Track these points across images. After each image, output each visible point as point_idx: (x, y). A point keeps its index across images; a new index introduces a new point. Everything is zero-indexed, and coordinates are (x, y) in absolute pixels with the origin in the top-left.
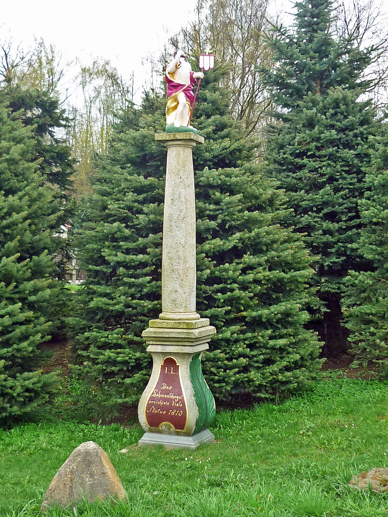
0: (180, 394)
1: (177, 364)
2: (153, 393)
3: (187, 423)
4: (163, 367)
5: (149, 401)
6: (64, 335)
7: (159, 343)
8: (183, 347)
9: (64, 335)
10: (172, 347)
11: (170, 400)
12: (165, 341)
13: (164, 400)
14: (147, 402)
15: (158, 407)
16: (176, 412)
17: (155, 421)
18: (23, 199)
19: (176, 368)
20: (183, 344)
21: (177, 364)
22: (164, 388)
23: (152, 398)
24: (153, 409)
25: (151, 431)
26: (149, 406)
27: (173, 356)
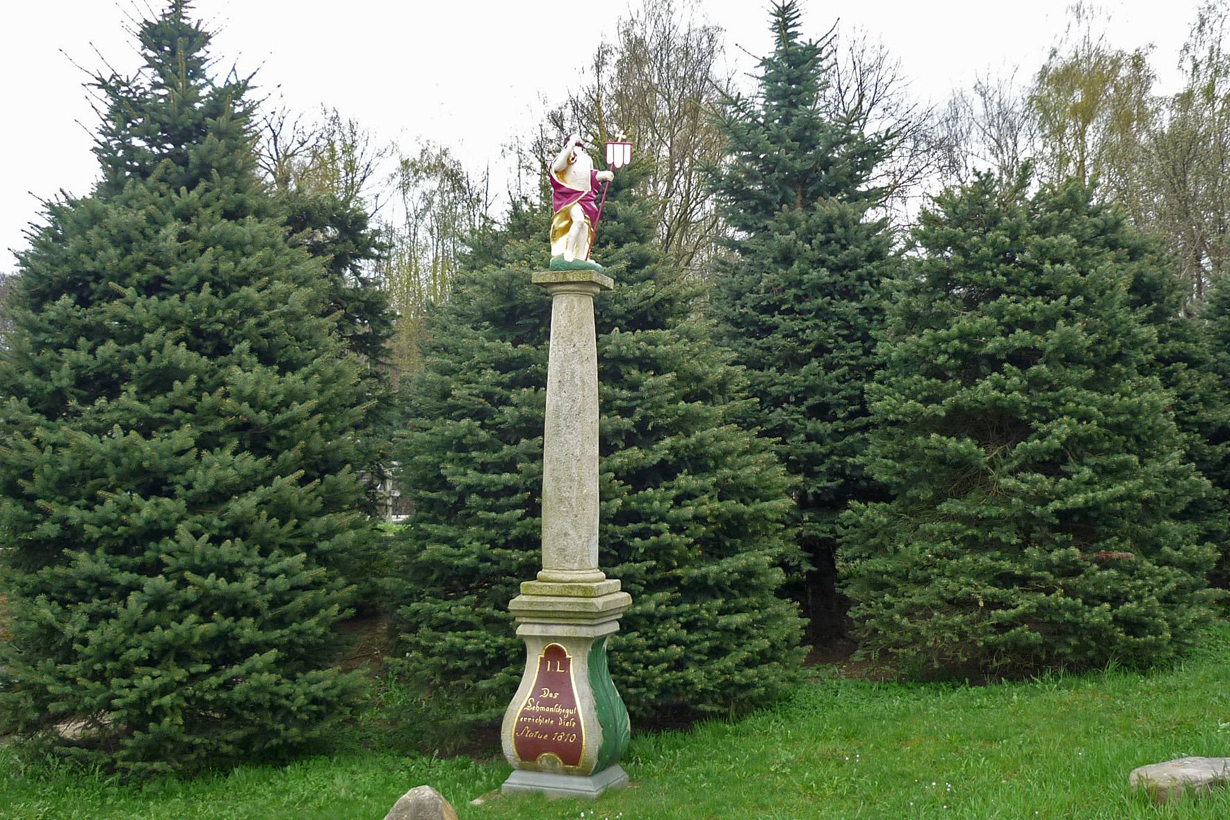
0: (572, 705)
2: (527, 705)
8: (578, 628)
11: (555, 717)
13: (546, 715)
15: (534, 727)
17: (529, 752)
23: (524, 714)
25: (522, 768)
26: (520, 727)
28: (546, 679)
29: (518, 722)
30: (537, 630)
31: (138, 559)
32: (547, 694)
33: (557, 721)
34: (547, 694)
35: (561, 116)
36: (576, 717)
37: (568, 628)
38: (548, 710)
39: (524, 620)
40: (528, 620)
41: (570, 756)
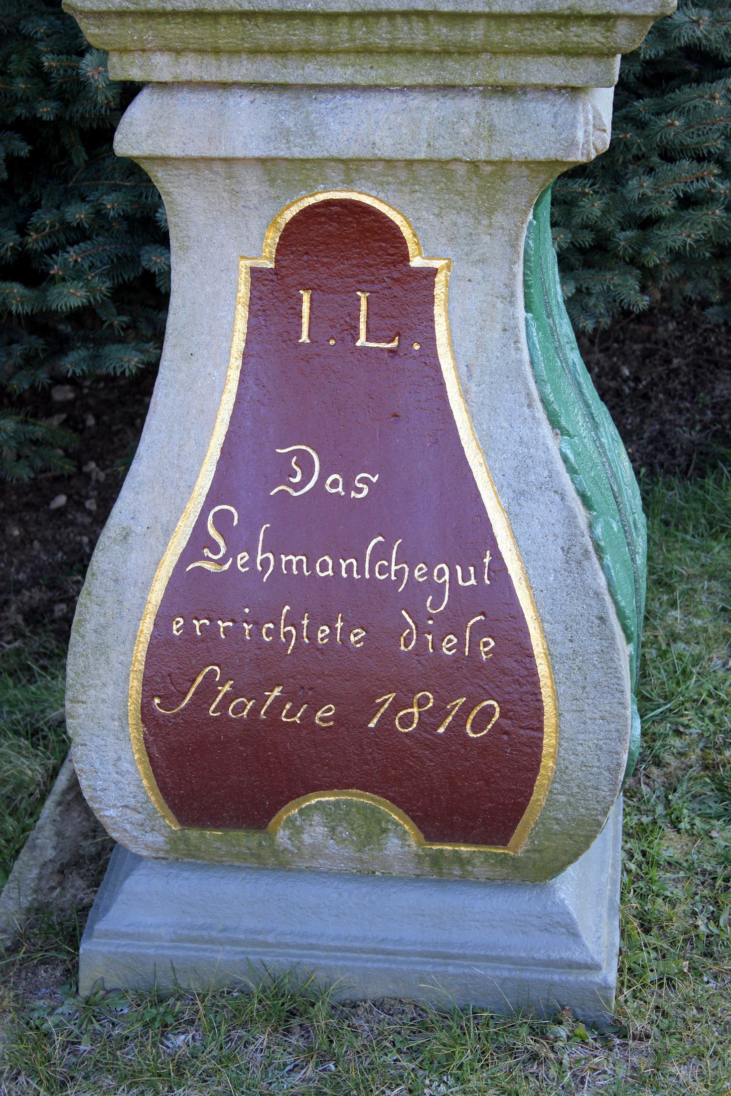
0: (469, 535)
1: (416, 262)
2: (199, 541)
3: (539, 796)
4: (271, 293)
5: (163, 619)
6: (623, 217)
7: (242, 70)
8: (501, 111)
9: (623, 217)
10: (375, 104)
11: (371, 602)
12: (308, 52)
13: (320, 600)
14: (147, 626)
15: (259, 667)
16: (439, 712)
17: (223, 778)
18: (183, 1030)
19: (408, 296)
20: (503, 72)
21: (416, 262)
22: (299, 486)
23: (188, 590)
24: (208, 690)
25: (179, 856)
26: (168, 670)
27: (380, 186)
28: (288, 385)
29: (160, 643)
30: (246, 126)
31: (676, 876)
32: (310, 477)
33: (384, 635)
34: (310, 477)
35: (671, 291)
36: (495, 604)
37: (436, 108)
38: (326, 567)
39: (162, 67)
40: (191, 68)
41: (473, 795)
